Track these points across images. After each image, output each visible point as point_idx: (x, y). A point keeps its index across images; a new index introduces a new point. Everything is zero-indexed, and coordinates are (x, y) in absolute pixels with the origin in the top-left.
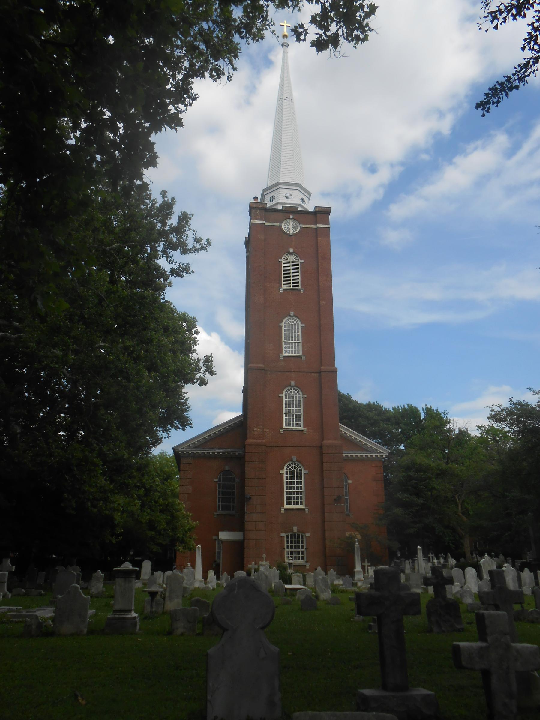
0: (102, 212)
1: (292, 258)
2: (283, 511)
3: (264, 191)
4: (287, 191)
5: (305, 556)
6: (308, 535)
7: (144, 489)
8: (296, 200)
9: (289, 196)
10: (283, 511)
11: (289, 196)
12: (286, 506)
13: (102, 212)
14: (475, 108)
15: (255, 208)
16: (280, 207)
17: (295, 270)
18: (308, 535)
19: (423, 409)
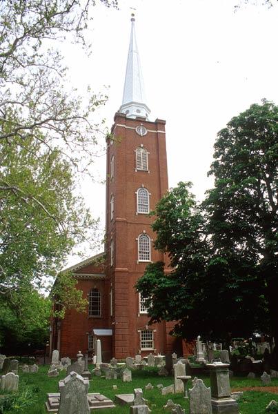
0: (53, 198)
1: (142, 151)
2: (139, 316)
3: (121, 107)
4: (137, 108)
5: (153, 345)
6: (155, 331)
7: (41, 291)
8: (142, 114)
9: (138, 111)
10: (139, 316)
11: (138, 111)
12: (141, 312)
13: (53, 198)
14: (253, 103)
15: (119, 116)
16: (134, 118)
17: (145, 159)
18: (155, 331)
19: (94, 4)
